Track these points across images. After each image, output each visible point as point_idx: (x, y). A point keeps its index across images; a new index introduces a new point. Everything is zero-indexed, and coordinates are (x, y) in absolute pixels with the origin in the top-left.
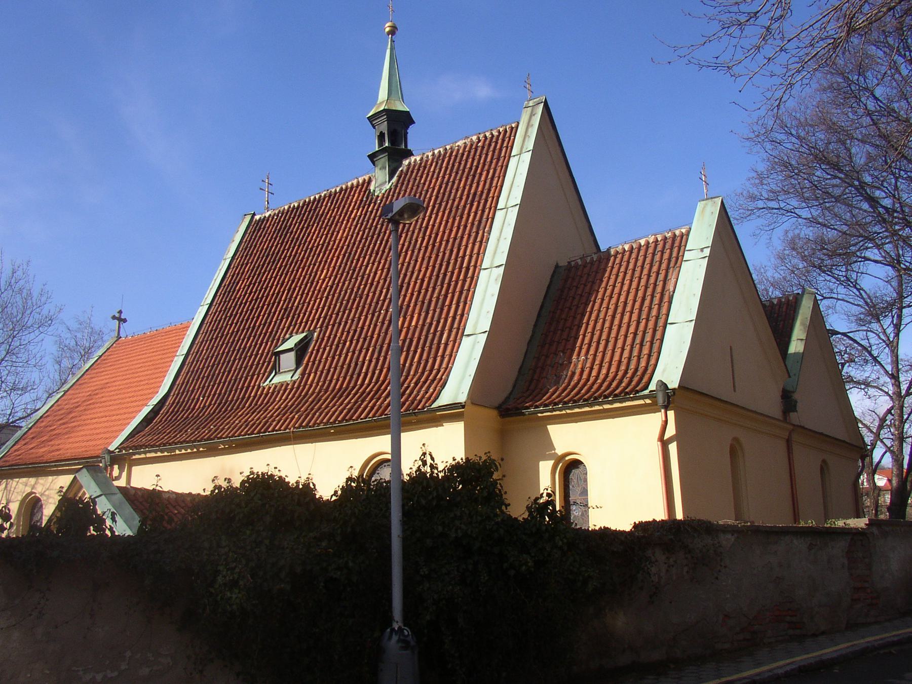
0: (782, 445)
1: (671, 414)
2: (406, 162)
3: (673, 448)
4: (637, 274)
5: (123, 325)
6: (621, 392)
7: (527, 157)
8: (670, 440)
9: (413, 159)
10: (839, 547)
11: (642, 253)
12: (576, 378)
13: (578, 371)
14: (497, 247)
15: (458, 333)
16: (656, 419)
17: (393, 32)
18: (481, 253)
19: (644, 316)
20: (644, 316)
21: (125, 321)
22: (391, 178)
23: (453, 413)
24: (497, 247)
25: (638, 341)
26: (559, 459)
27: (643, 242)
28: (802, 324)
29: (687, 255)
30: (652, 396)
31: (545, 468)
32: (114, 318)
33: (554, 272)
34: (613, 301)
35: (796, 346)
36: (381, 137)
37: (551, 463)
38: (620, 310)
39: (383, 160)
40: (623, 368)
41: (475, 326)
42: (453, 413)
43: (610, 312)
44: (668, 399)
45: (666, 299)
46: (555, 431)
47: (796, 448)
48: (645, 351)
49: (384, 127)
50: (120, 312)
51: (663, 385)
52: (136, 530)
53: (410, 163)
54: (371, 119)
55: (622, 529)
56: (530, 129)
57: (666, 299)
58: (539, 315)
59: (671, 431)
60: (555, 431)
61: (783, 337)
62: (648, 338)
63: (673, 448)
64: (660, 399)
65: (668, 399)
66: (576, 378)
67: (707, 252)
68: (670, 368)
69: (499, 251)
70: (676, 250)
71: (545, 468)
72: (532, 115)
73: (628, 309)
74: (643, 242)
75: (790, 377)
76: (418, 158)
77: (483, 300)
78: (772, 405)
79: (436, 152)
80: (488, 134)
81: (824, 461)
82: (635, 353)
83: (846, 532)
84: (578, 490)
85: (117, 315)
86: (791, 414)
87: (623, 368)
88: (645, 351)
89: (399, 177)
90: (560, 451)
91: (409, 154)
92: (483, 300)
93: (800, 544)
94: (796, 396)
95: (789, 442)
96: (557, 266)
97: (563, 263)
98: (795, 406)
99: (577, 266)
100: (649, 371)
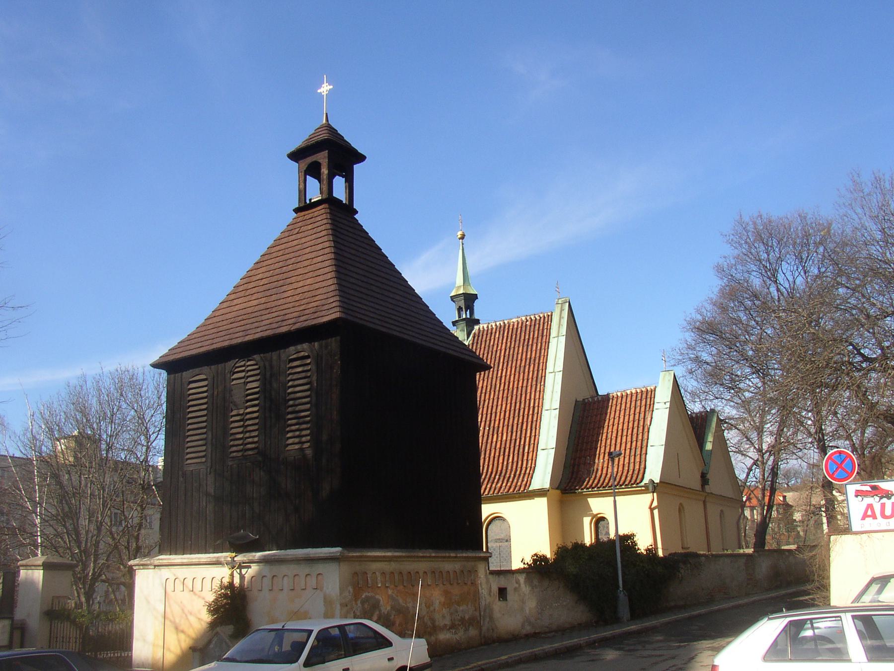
1: (655, 494)
2: (476, 327)
3: (656, 512)
4: (627, 413)
6: (629, 482)
7: (563, 340)
8: (655, 508)
9: (481, 326)
10: (743, 561)
11: (629, 399)
12: (599, 472)
13: (600, 468)
16: (649, 497)
17: (462, 238)
18: (541, 398)
19: (634, 439)
20: (634, 439)
22: (468, 338)
23: (541, 493)
25: (633, 453)
26: (594, 516)
27: (629, 392)
29: (656, 406)
30: (646, 486)
31: (587, 520)
34: (615, 427)
35: (709, 446)
36: (460, 309)
37: (590, 518)
38: (620, 434)
39: (463, 325)
40: (626, 468)
42: (541, 493)
43: (614, 435)
44: (653, 487)
45: (646, 430)
46: (592, 501)
47: (708, 505)
48: (638, 459)
49: (462, 304)
51: (652, 481)
52: (665, 556)
54: (452, 298)
57: (646, 430)
59: (655, 504)
60: (592, 501)
61: (701, 442)
62: (638, 452)
63: (656, 512)
64: (651, 488)
65: (653, 487)
66: (599, 472)
67: (668, 405)
68: (654, 471)
70: (648, 400)
71: (587, 520)
72: (562, 310)
73: (625, 433)
74: (629, 392)
76: (485, 326)
77: (549, 429)
78: (696, 484)
79: (498, 324)
80: (532, 317)
81: (722, 511)
82: (632, 460)
83: (745, 555)
84: (604, 533)
87: (626, 468)
88: (638, 459)
89: (474, 337)
90: (595, 512)
91: (477, 322)
92: (549, 429)
93: (727, 560)
94: (708, 476)
95: (704, 502)
97: (580, 399)
99: (589, 403)
100: (641, 471)
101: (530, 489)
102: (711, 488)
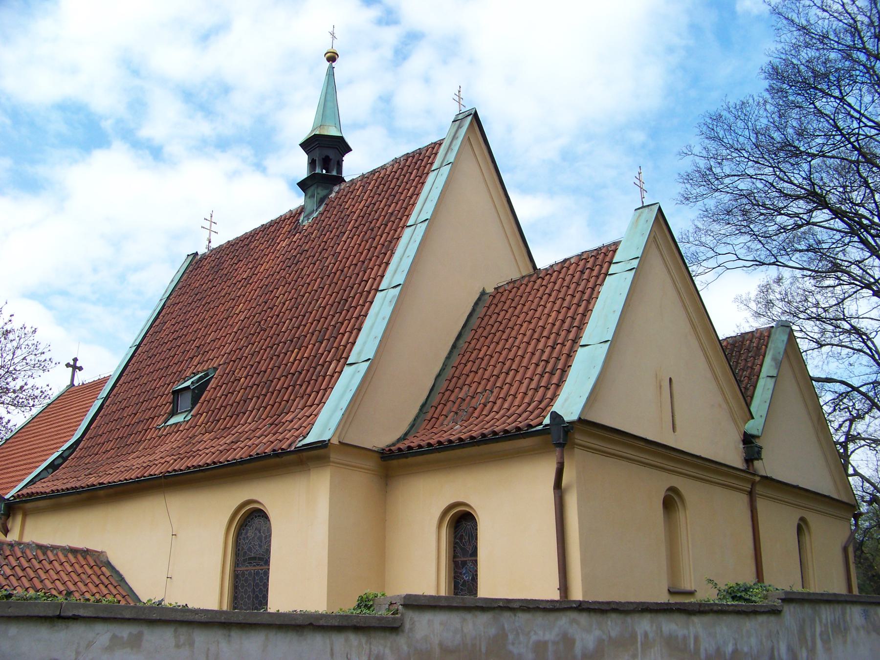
0: (745, 498)
2: (336, 188)
5: (78, 372)
14: (398, 266)
15: (342, 359)
21: (80, 369)
24: (398, 266)
28: (774, 359)
32: (68, 365)
33: (479, 299)
41: (360, 353)
47: (761, 504)
50: (75, 360)
51: (556, 416)
53: (340, 190)
55: (313, 611)
56: (454, 142)
58: (454, 346)
69: (400, 270)
75: (670, 379)
81: (802, 519)
85: (72, 363)
86: (756, 462)
96: (483, 293)
98: (759, 453)
101: (309, 439)
102: (767, 466)
